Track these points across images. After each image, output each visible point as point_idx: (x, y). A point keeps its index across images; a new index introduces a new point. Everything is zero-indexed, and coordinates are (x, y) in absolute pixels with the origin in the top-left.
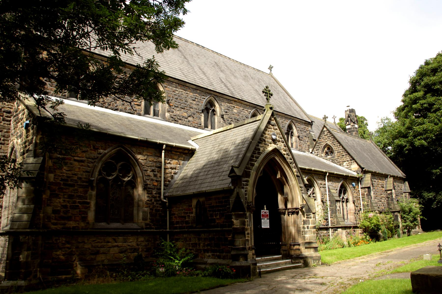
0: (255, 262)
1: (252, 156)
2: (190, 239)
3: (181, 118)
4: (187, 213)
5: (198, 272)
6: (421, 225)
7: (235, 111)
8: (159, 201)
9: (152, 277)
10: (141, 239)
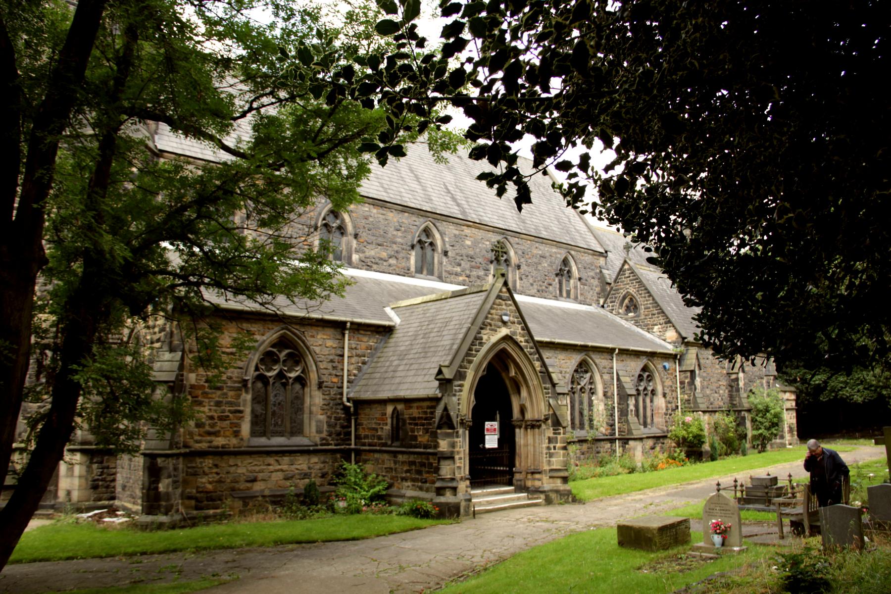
0: (468, 497)
1: (470, 349)
2: (383, 461)
3: (377, 260)
4: (379, 424)
5: (393, 508)
6: (798, 431)
8: (340, 404)
9: (330, 514)
10: (315, 459)
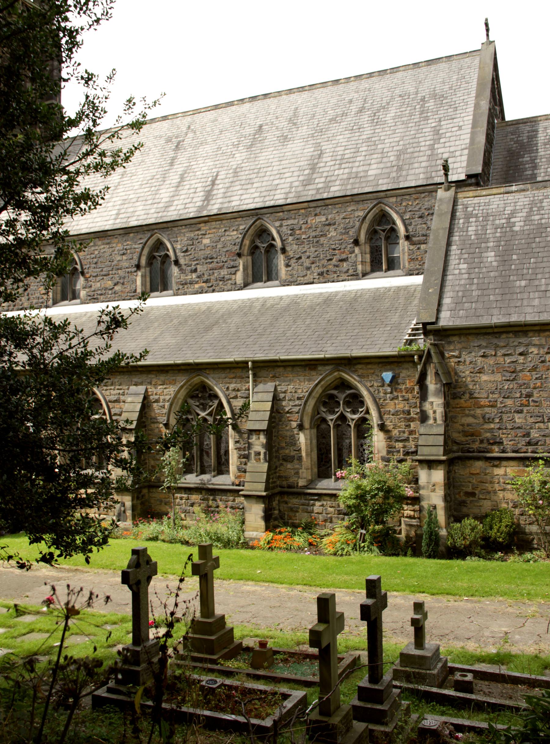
3: (104, 292)
7: (206, 241)
